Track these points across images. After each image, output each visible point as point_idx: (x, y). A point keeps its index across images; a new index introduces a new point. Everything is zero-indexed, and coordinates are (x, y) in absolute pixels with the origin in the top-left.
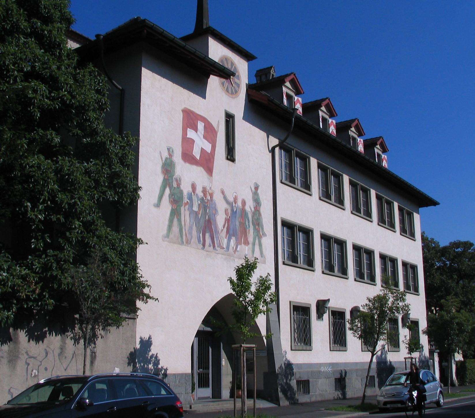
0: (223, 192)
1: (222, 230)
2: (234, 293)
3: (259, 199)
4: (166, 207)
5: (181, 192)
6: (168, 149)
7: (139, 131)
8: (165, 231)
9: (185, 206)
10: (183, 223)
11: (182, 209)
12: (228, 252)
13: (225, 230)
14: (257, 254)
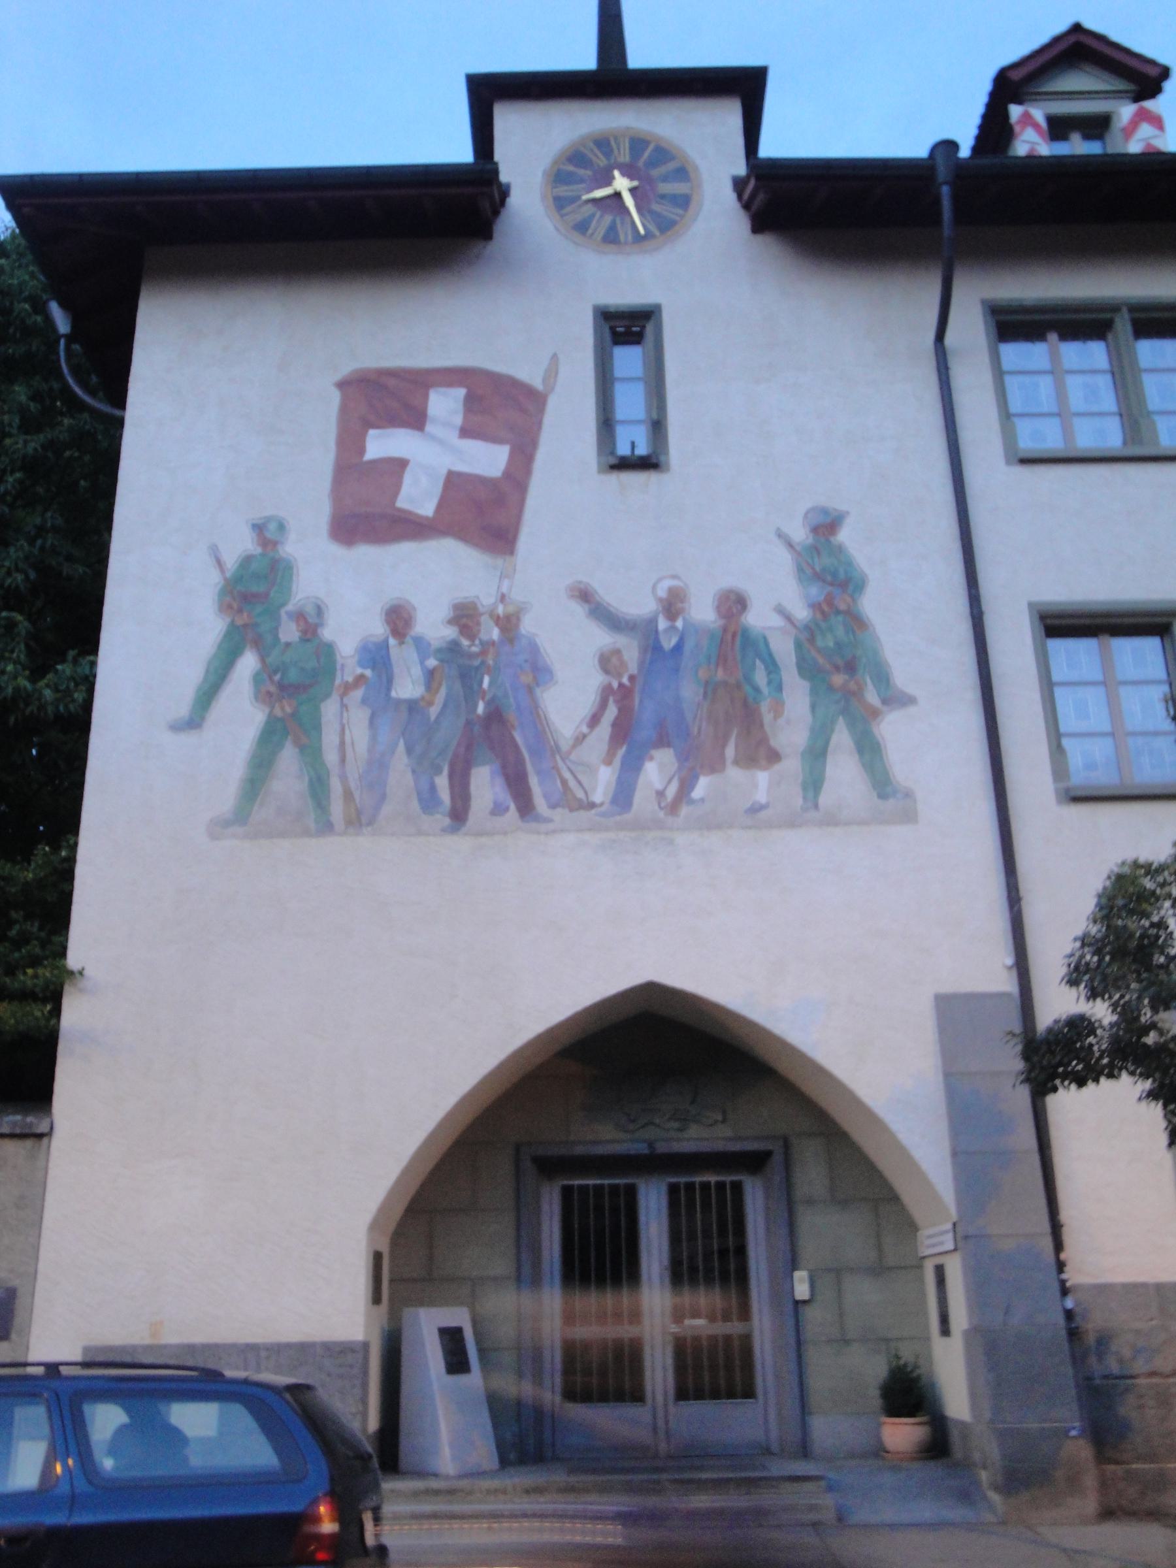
0: (584, 595)
1: (580, 739)
2: (730, 751)
3: (849, 563)
4: (241, 714)
5: (327, 651)
6: (259, 528)
7: (127, 381)
8: (227, 798)
9: (342, 696)
10: (331, 757)
11: (330, 709)
12: (627, 817)
13: (604, 729)
14: (672, 1409)
